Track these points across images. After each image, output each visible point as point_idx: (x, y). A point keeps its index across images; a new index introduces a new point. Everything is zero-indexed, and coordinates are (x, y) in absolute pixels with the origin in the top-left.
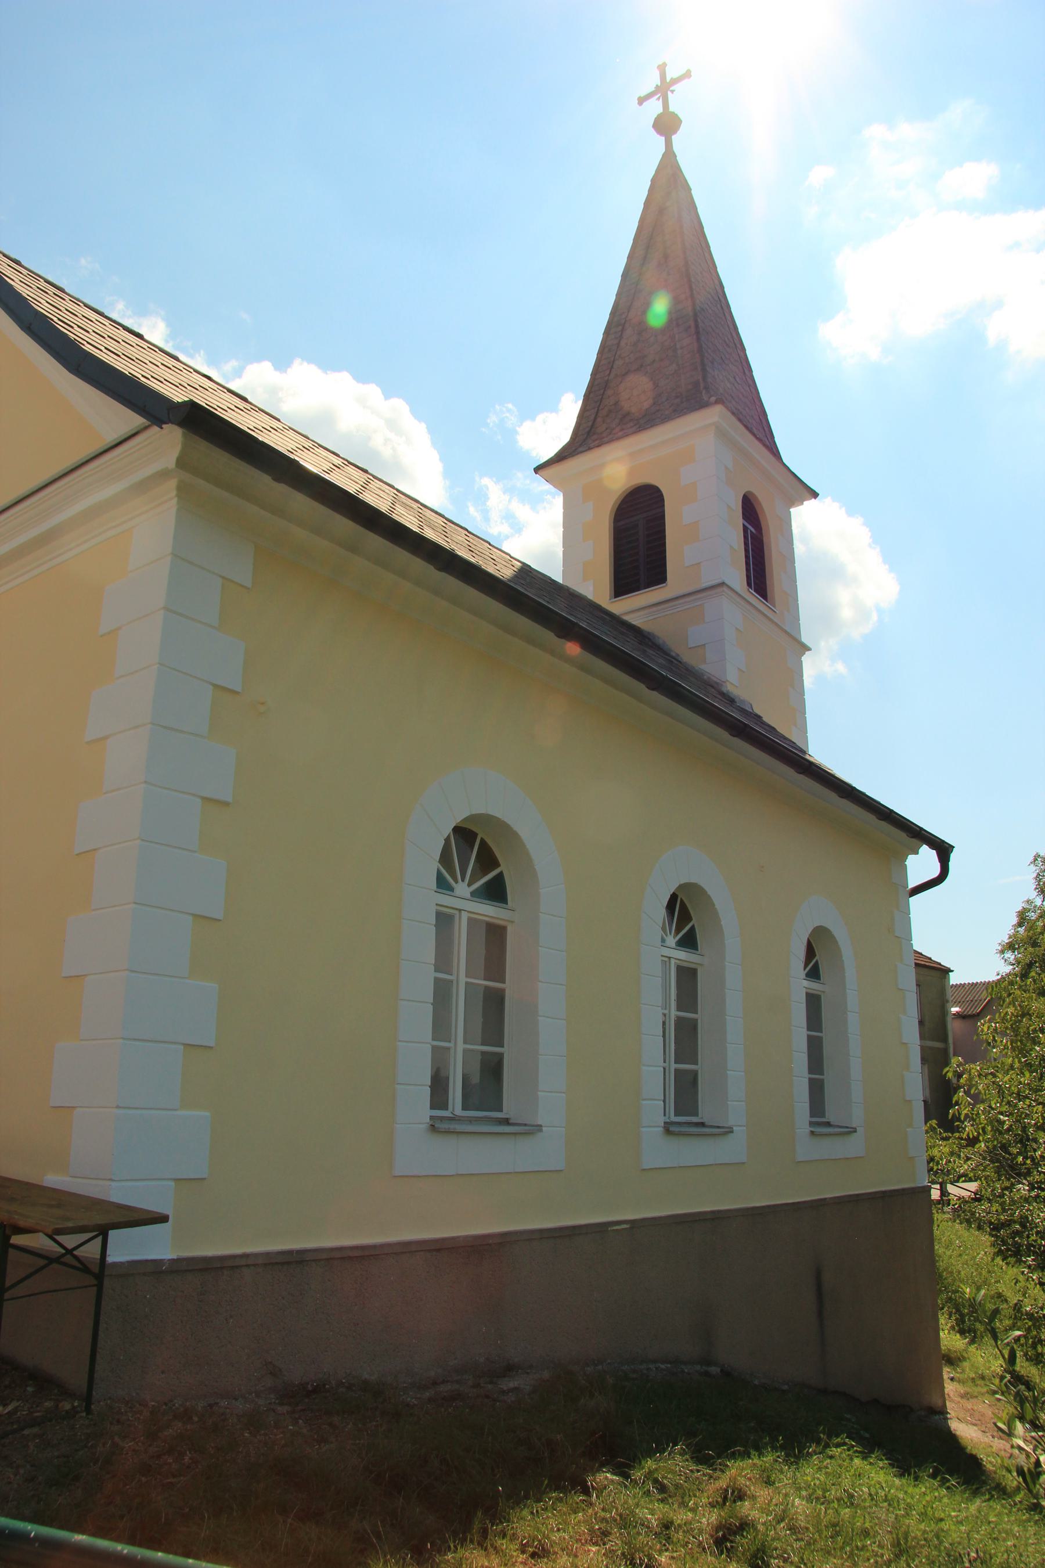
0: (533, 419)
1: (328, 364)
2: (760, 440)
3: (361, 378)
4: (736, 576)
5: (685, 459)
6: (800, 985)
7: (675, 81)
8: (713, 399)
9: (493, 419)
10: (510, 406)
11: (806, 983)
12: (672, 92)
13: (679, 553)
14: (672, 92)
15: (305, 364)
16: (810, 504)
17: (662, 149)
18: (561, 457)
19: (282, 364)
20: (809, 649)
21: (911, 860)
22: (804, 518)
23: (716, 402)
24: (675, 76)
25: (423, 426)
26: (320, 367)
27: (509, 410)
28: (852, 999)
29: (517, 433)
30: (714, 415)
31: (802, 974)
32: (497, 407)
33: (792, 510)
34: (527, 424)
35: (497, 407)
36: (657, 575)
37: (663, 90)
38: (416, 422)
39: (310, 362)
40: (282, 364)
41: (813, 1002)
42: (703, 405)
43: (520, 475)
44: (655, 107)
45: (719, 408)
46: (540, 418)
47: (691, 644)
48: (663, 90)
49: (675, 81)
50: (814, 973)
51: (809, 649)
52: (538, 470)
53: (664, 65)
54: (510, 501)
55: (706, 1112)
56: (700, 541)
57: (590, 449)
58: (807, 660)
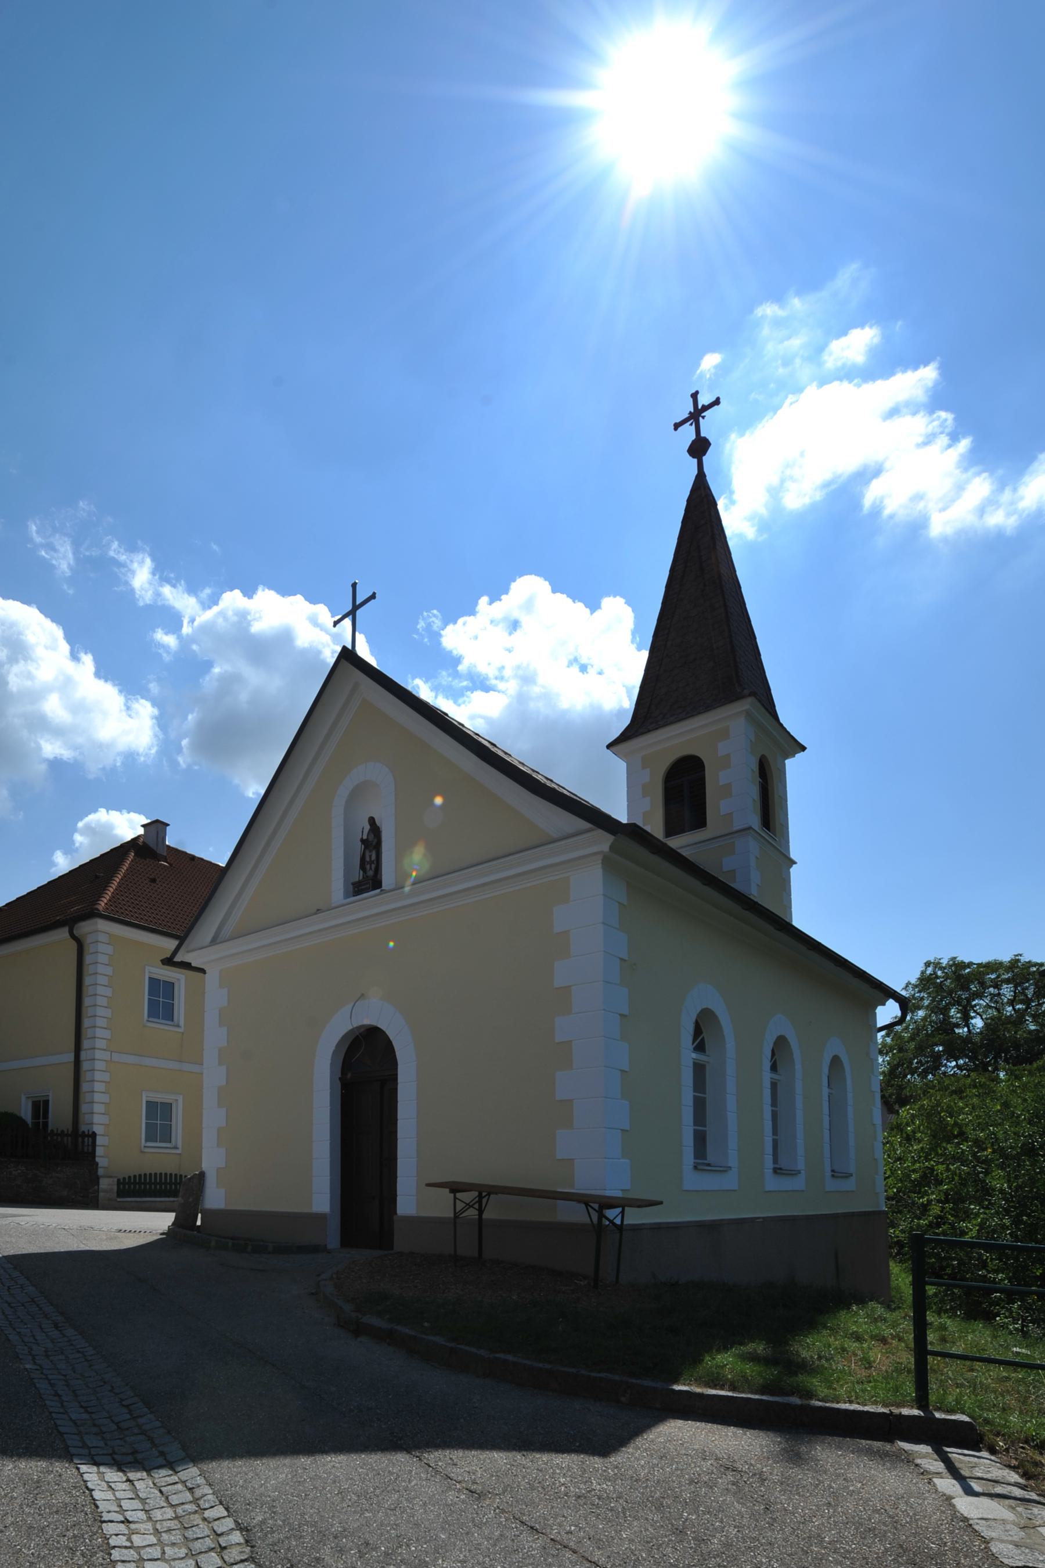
0: (455, 623)
1: (285, 591)
2: (767, 710)
3: (312, 599)
4: (755, 821)
5: (716, 736)
6: (689, 1056)
7: (706, 408)
8: (746, 692)
9: (421, 625)
10: (435, 612)
11: (694, 1055)
12: (703, 417)
13: (717, 806)
14: (703, 417)
15: (267, 590)
16: (800, 756)
17: (695, 472)
18: (626, 736)
19: (249, 592)
20: (795, 863)
21: (880, 1010)
22: (794, 767)
23: (750, 695)
24: (706, 403)
25: (299, 598)
26: (278, 593)
27: (435, 616)
28: (730, 1068)
29: (440, 636)
30: (746, 705)
31: (691, 1047)
32: (425, 614)
33: (787, 762)
34: (450, 628)
35: (425, 614)
36: (699, 821)
37: (696, 415)
38: (307, 603)
39: (270, 588)
40: (249, 592)
41: (699, 1070)
42: (736, 697)
43: (444, 673)
44: (688, 433)
45: (751, 700)
46: (461, 621)
47: (724, 870)
48: (696, 415)
49: (706, 408)
50: (700, 1048)
51: (795, 863)
52: (609, 747)
53: (697, 392)
54: (436, 697)
55: (711, 1158)
56: (729, 794)
57: (649, 731)
58: (794, 870)
